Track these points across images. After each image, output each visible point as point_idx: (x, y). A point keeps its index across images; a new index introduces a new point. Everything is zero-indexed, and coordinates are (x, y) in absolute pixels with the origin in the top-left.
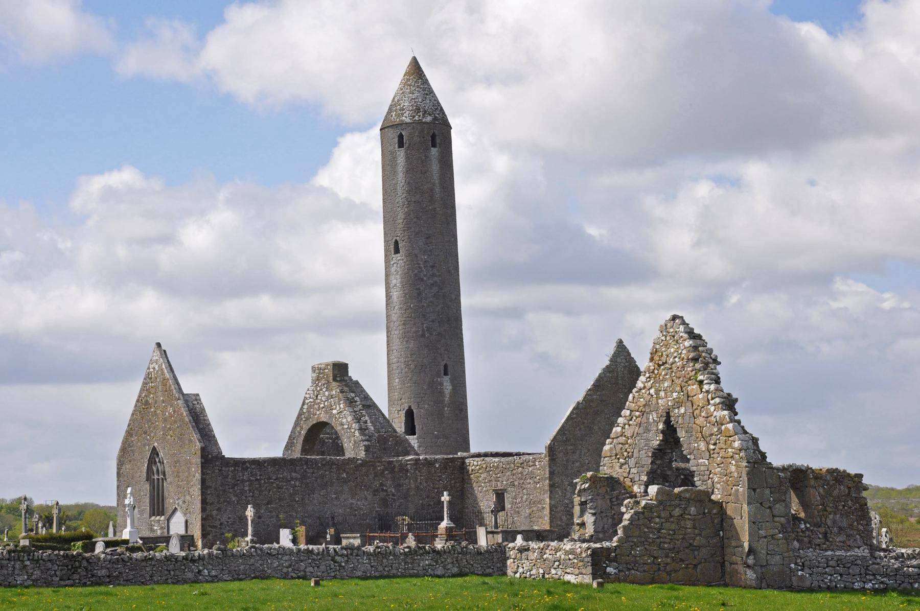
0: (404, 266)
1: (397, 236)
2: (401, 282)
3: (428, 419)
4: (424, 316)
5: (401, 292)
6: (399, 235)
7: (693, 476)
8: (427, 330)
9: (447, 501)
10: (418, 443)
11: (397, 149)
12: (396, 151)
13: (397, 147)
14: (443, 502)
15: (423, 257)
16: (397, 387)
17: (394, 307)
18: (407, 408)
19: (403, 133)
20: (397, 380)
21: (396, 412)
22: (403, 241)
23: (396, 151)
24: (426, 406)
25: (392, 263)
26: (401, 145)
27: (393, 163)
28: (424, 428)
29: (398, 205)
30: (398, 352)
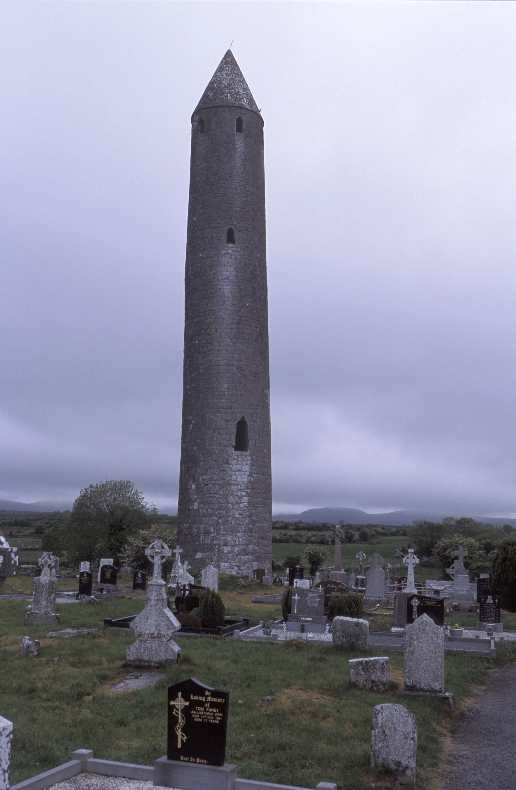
1: (233, 225)
2: (236, 276)
13: (235, 130)
17: (224, 302)
18: (240, 419)
19: (243, 118)
20: (225, 386)
24: (259, 420)
25: (223, 252)
26: (239, 129)
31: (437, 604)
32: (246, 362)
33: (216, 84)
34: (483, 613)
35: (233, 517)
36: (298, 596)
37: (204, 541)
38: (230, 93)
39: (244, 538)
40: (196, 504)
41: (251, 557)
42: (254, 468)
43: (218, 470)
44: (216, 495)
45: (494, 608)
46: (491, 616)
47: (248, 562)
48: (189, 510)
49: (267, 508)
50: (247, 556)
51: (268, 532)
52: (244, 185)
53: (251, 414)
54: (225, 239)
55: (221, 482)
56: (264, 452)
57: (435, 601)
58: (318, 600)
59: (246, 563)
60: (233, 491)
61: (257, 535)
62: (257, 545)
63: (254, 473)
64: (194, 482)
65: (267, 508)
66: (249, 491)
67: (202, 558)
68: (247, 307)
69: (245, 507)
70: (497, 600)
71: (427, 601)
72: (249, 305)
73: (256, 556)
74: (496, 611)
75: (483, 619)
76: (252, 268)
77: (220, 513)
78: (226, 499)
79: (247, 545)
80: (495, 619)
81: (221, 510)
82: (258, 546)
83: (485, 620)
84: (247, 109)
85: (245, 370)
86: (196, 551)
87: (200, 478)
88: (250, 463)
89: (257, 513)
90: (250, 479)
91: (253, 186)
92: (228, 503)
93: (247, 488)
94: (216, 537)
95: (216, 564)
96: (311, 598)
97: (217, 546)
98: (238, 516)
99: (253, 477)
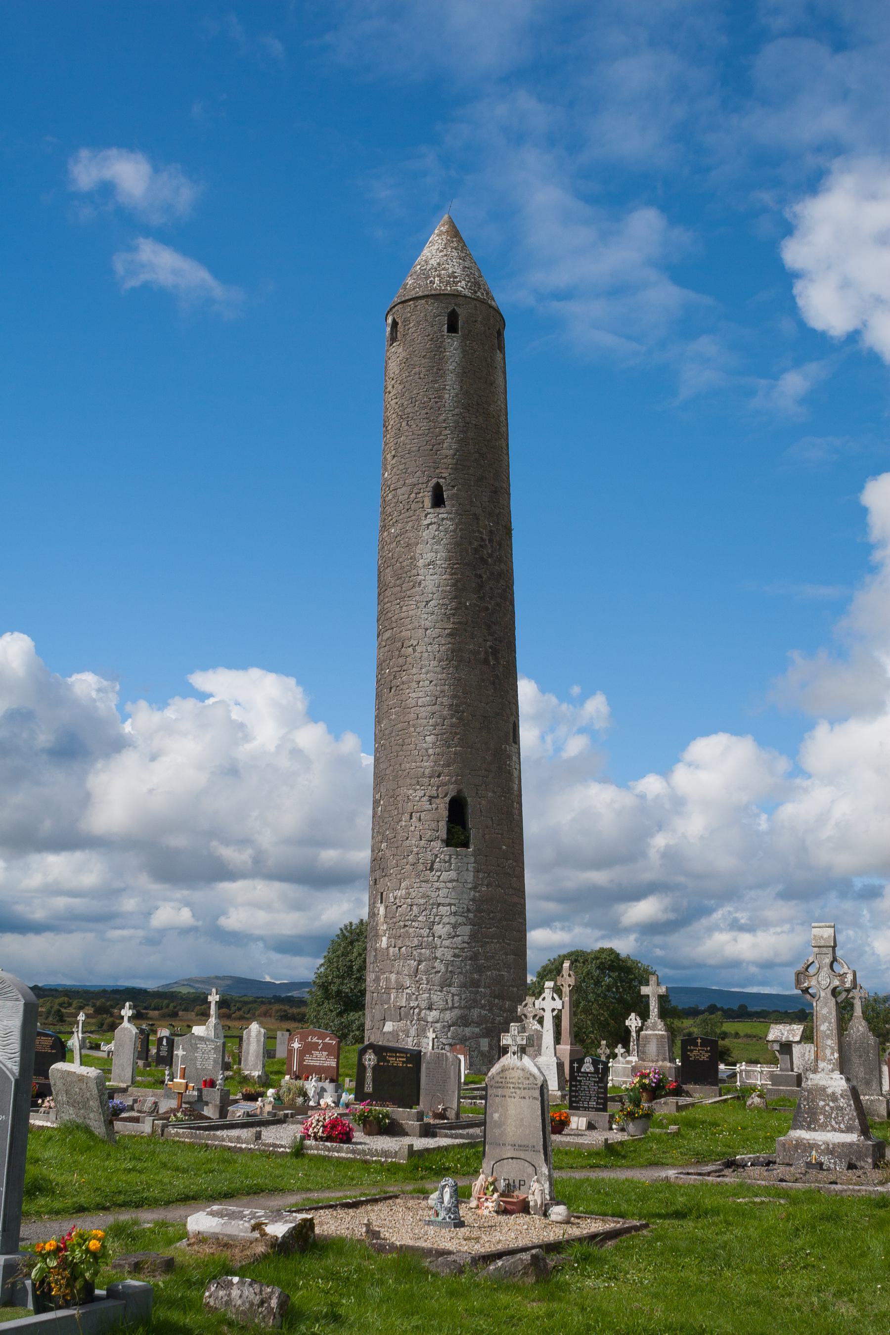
0: (454, 531)
1: (441, 477)
3: (492, 820)
4: (489, 627)
5: (448, 577)
6: (443, 475)
7: (361, 1011)
8: (491, 653)
9: (216, 1002)
10: (474, 863)
11: (445, 333)
12: (443, 336)
13: (446, 330)
14: (210, 1002)
15: (487, 523)
16: (431, 751)
21: (426, 798)
22: (453, 487)
23: (443, 336)
24: (490, 794)
25: (426, 522)
26: (452, 328)
27: (435, 355)
28: (487, 837)
29: (444, 425)
30: (436, 685)
31: (407, 1062)
32: (465, 698)
33: (419, 267)
34: (576, 1091)
35: (442, 961)
36: (184, 1049)
37: (397, 1002)
38: (439, 276)
39: (463, 996)
40: (384, 939)
41: (477, 1030)
42: (481, 875)
43: (418, 881)
44: (413, 923)
45: (595, 1082)
46: (591, 1097)
47: (470, 1038)
48: (376, 950)
49: (509, 944)
50: (470, 1028)
51: (513, 986)
52: (461, 413)
53: (475, 785)
54: (428, 502)
55: (422, 901)
56: (501, 848)
57: (403, 1057)
58: (213, 1056)
59: (466, 1040)
60: (442, 916)
61: (488, 991)
62: (487, 1008)
63: (482, 885)
64: (381, 902)
65: (509, 944)
66: (471, 915)
67: (393, 1030)
68: (466, 608)
69: (463, 942)
70: (600, 1066)
71: (389, 1056)
72: (470, 604)
73: (485, 1028)
74: (600, 1087)
75: (574, 1105)
76: (476, 544)
77: (420, 953)
78: (431, 929)
79: (469, 1008)
80: (597, 1103)
81: (422, 949)
82: (490, 1010)
83: (580, 1107)
84: (465, 296)
85: (463, 712)
86: (384, 1019)
87: (391, 895)
88: (473, 867)
89: (488, 952)
90: (474, 895)
91: (478, 414)
92: (434, 936)
93: (469, 910)
94: (414, 994)
95: (415, 1041)
96: (203, 1053)
97: (417, 1010)
98: (452, 959)
99: (479, 892)
